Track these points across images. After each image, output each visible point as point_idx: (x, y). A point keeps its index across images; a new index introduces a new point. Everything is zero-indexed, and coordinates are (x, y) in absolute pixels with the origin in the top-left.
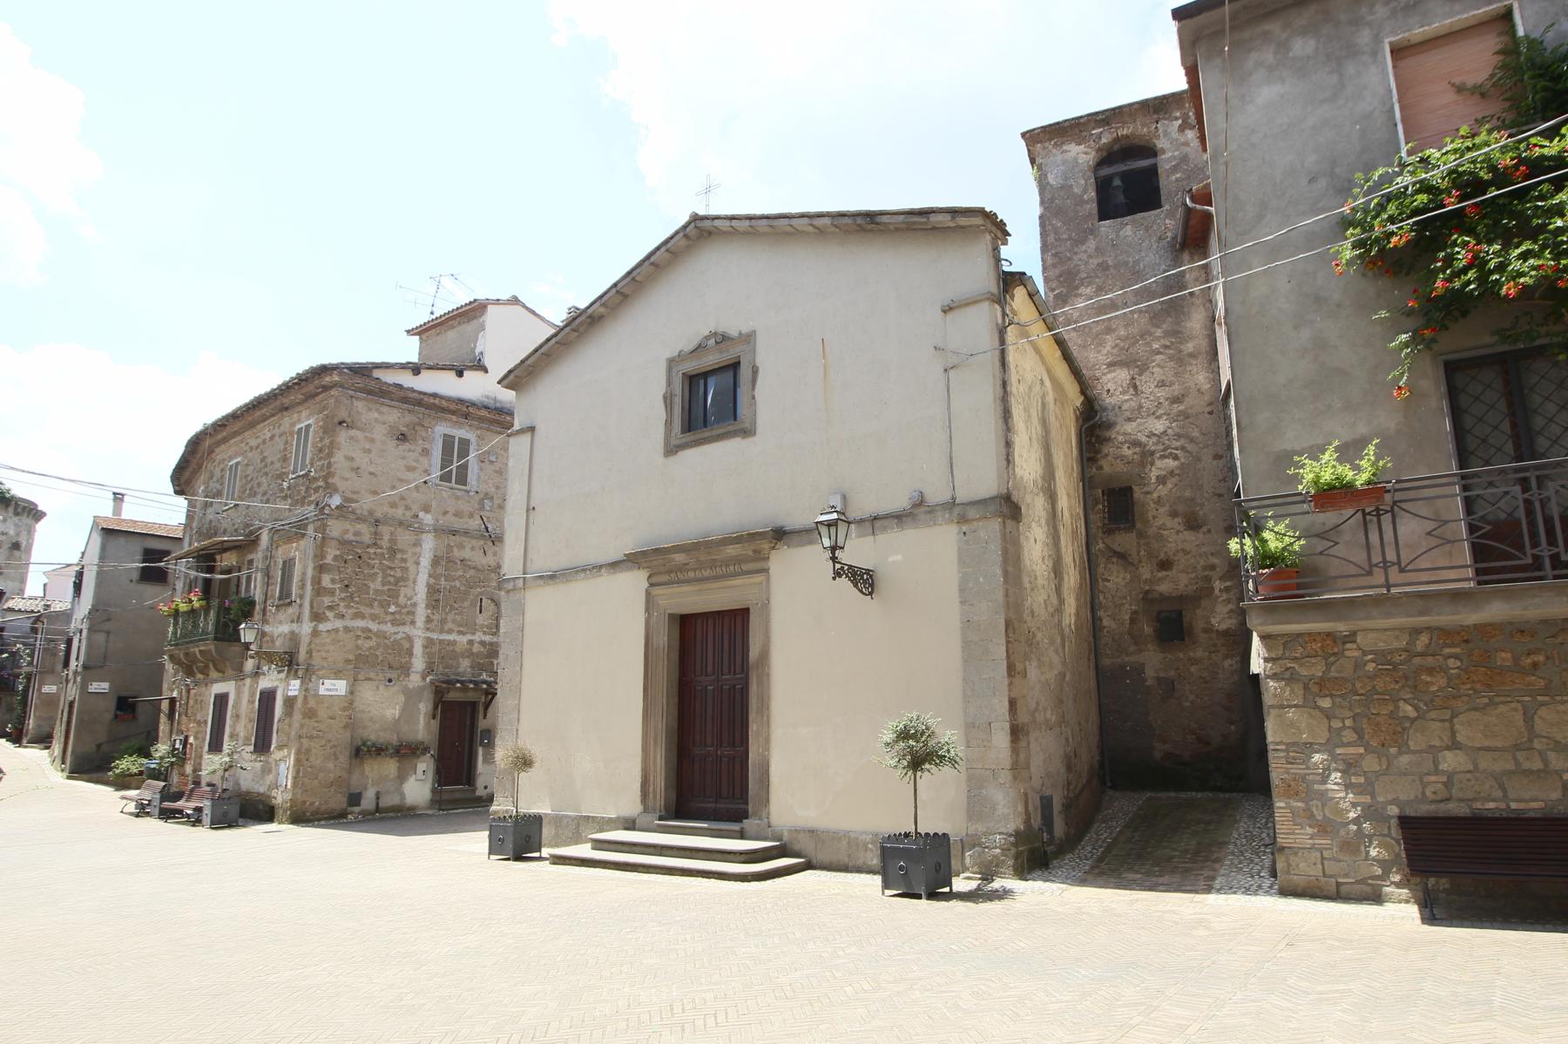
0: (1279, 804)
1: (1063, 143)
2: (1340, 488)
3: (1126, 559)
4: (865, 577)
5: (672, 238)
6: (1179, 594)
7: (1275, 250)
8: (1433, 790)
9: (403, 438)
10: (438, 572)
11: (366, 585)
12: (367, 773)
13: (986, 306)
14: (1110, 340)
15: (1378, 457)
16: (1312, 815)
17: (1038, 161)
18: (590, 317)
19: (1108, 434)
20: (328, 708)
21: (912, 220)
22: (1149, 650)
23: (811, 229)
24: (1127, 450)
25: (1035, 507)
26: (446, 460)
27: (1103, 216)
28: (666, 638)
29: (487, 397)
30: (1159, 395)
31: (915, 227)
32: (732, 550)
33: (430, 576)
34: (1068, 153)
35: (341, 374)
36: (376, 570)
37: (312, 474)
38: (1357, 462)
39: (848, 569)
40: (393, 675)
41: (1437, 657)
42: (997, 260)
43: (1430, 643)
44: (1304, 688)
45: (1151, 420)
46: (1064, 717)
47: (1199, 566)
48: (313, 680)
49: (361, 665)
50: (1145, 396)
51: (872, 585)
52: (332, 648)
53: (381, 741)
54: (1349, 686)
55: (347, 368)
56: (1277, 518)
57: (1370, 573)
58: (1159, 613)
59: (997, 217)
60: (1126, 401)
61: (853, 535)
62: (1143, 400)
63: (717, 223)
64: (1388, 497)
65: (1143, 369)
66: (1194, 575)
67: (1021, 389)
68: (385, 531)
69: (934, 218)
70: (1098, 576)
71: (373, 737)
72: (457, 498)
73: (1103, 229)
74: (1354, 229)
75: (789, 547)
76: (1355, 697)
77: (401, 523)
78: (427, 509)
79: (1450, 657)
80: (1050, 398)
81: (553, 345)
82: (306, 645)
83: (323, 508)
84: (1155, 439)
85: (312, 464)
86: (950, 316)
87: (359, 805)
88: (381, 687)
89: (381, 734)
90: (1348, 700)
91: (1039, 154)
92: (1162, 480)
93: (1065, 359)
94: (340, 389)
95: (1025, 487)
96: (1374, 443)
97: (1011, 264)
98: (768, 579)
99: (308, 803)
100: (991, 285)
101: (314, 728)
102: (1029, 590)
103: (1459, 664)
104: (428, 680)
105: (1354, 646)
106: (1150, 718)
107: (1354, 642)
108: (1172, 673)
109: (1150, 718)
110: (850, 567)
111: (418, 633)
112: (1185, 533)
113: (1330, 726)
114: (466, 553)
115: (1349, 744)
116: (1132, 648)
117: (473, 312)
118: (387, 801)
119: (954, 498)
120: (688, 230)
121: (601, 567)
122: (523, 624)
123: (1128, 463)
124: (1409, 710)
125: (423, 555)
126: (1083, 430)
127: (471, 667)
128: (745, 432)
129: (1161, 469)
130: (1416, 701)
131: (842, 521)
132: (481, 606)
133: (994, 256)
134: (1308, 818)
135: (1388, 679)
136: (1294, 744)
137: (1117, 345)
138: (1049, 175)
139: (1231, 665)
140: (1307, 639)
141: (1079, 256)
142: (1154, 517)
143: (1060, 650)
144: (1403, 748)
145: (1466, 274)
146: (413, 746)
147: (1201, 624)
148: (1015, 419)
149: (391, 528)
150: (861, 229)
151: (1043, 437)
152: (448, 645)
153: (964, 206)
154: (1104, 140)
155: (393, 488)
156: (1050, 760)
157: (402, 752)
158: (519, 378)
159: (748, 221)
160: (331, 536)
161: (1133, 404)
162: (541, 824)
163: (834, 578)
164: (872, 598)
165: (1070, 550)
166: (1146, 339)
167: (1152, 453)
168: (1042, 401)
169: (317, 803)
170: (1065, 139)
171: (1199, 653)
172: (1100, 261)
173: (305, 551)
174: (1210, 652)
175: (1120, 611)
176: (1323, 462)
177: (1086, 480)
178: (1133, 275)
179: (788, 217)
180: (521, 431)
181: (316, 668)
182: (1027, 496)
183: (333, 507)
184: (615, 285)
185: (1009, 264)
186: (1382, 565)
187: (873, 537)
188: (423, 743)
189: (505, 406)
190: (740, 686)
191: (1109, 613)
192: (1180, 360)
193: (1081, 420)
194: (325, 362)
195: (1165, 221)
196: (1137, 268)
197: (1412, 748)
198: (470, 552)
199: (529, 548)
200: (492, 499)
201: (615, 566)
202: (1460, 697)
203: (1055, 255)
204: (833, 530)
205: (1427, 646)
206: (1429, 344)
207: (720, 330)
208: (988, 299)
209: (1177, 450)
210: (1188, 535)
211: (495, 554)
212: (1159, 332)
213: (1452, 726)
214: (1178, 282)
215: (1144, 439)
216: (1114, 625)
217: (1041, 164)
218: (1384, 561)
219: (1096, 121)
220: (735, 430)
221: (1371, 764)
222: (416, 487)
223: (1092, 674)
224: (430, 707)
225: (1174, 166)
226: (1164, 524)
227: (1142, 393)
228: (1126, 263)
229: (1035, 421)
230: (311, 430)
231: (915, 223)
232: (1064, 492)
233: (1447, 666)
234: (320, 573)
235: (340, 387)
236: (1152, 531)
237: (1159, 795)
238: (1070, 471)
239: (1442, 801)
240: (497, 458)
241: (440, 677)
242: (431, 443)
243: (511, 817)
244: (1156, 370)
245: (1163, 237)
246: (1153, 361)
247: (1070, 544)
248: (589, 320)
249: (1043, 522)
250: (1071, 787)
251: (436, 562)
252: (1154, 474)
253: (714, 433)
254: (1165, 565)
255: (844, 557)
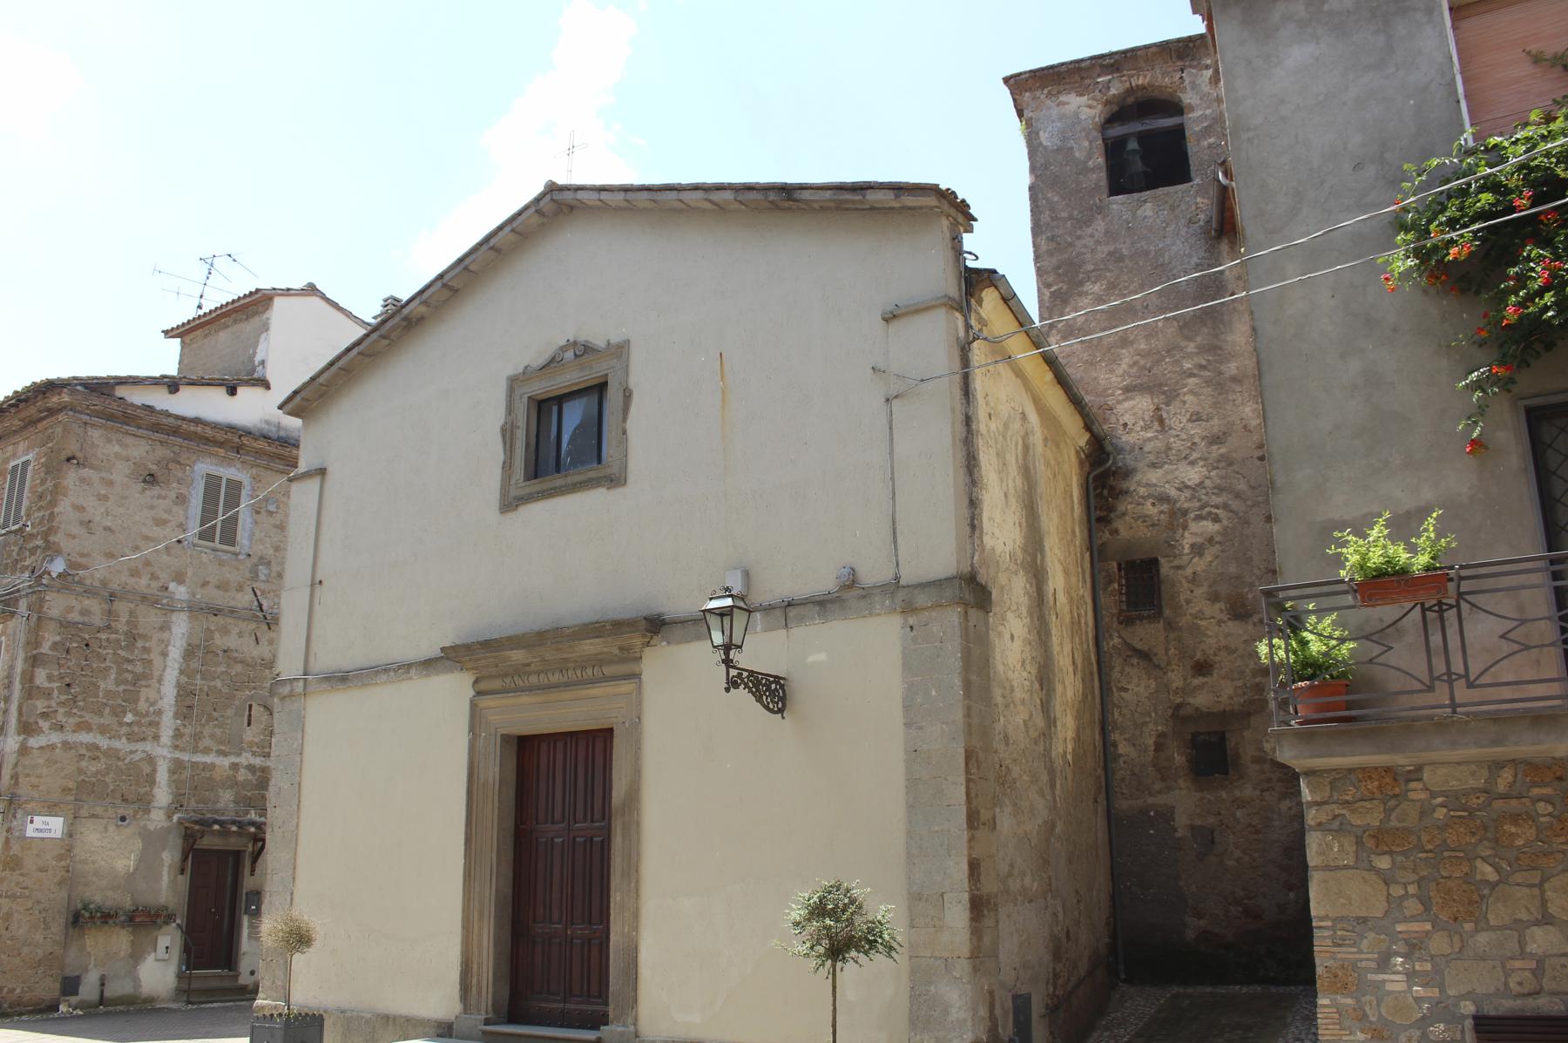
0: (1322, 1001)
1: (1059, 92)
2: (1393, 575)
3: (1151, 660)
4: (773, 686)
5: (520, 213)
6: (1222, 709)
7: (1314, 255)
8: (1519, 980)
9: (151, 479)
10: (192, 667)
11: (94, 684)
12: (89, 949)
13: (941, 315)
14: (1126, 357)
15: (1440, 534)
16: (1365, 1015)
17: (1027, 114)
18: (406, 319)
19: (1125, 485)
20: (37, 855)
21: (842, 197)
22: (1181, 789)
23: (708, 205)
24: (1151, 507)
25: (1013, 590)
26: (208, 512)
27: (1116, 188)
28: (497, 769)
29: (267, 422)
30: (1192, 432)
31: (847, 206)
32: (589, 647)
33: (182, 672)
34: (1066, 106)
35: (73, 392)
36: (108, 663)
37: (28, 529)
38: (1413, 540)
39: (748, 677)
40: (128, 811)
41: (1523, 800)
42: (958, 251)
43: (1515, 782)
44: (1357, 843)
45: (1183, 466)
46: (1050, 885)
47: (1247, 671)
48: (19, 816)
49: (84, 797)
50: (1172, 432)
51: (783, 699)
52: (45, 771)
53: (109, 903)
54: (1413, 839)
55: (80, 384)
56: (1321, 612)
57: (1430, 688)
58: (1195, 735)
59: (956, 197)
60: (1150, 439)
61: (759, 628)
62: (1172, 440)
63: (580, 195)
64: (1451, 586)
65: (1171, 396)
66: (1239, 683)
67: (993, 427)
68: (122, 608)
69: (871, 196)
70: (1112, 685)
71: (98, 898)
72: (221, 563)
73: (1115, 206)
74: (1406, 234)
75: (669, 643)
76: (1421, 855)
77: (144, 598)
78: (180, 578)
79: (1539, 800)
80: (1037, 438)
81: (355, 356)
82: (10, 767)
83: (40, 576)
84: (1188, 493)
85: (28, 516)
86: (895, 326)
87: (76, 993)
88: (111, 828)
89: (110, 893)
90: (1412, 858)
91: (1028, 105)
92: (1198, 550)
93: (1059, 383)
94: (71, 413)
95: (998, 561)
96: (1434, 515)
97: (977, 258)
98: (640, 688)
99: (6, 989)
100: (951, 286)
101: (17, 884)
102: (1001, 708)
103: (1550, 809)
104: (175, 818)
105: (1419, 785)
106: (1182, 883)
107: (1419, 780)
108: (1212, 820)
109: (1182, 883)
110: (751, 673)
111: (163, 752)
112: (1230, 624)
113: (1389, 894)
114: (232, 641)
115: (1413, 918)
116: (1158, 786)
117: (255, 305)
118: (115, 989)
119: (897, 578)
120: (542, 203)
121: (410, 666)
122: (302, 744)
123: (1153, 525)
124: (1488, 872)
125: (172, 643)
126: (1091, 480)
127: (234, 801)
128: (612, 481)
129: (1196, 534)
130: (1497, 860)
131: (743, 607)
132: (250, 715)
133: (953, 248)
134: (1360, 1020)
135: (1462, 829)
136: (1342, 919)
137: (1135, 363)
138: (1041, 133)
139: (1290, 808)
140: (1360, 776)
141: (1083, 242)
142: (1188, 602)
143: (1047, 791)
144: (1481, 924)
145: (1542, 298)
146: (153, 912)
147: (1248, 752)
148: (983, 468)
149: (130, 605)
150: (775, 206)
151: (1024, 492)
152: (203, 770)
153: (912, 181)
154: (1113, 91)
155: (136, 548)
156: (1029, 944)
157: (138, 920)
158: (307, 401)
159: (622, 194)
160: (50, 616)
161: (1158, 444)
162: (322, 1026)
163: (727, 690)
164: (783, 718)
165: (1067, 649)
166: (1174, 356)
167: (1185, 513)
168: (1024, 442)
169: (18, 990)
170: (1062, 88)
171: (1248, 791)
172: (1112, 248)
173: (14, 635)
174: (1262, 791)
175: (1142, 732)
176: (1371, 539)
177: (1095, 549)
178: (1156, 268)
179: (676, 189)
180: (308, 475)
181: (23, 799)
182: (1000, 575)
183: (54, 575)
184: (441, 276)
185: (974, 258)
186: (1445, 678)
187: (785, 631)
188: (167, 908)
189: (293, 434)
190: (600, 839)
191: (1126, 736)
192: (1220, 385)
193: (1087, 465)
194: (53, 376)
195: (1193, 200)
196: (1161, 259)
197: (1492, 923)
198: (237, 639)
199: (314, 637)
200: (269, 564)
201: (428, 665)
202: (1552, 853)
203: (1052, 239)
204: (727, 620)
205: (1511, 785)
206: (1507, 384)
207: (582, 338)
208: (945, 305)
209: (1218, 508)
210: (1233, 627)
211: (271, 642)
212: (1191, 347)
213: (1543, 893)
214: (1214, 282)
215: (1173, 493)
216: (1133, 754)
217: (1031, 118)
218: (1449, 672)
219: (1102, 66)
220: (598, 478)
221: (1439, 943)
222: (167, 548)
223: (1101, 822)
224: (178, 856)
225: (1206, 127)
226: (1201, 611)
227: (1170, 429)
228: (1147, 253)
229: (1013, 470)
230: (30, 468)
231: (847, 201)
232: (1059, 568)
233: (1536, 811)
234: (33, 667)
235: (71, 410)
236: (1184, 621)
237: (1190, 990)
238: (1069, 537)
239: (1529, 994)
240: (278, 507)
241: (192, 814)
242: (188, 487)
243: (280, 1015)
244: (1189, 398)
245: (1194, 219)
246: (1185, 386)
247: (1067, 641)
248: (404, 323)
249: (1024, 611)
250: (1060, 982)
251: (189, 653)
252: (1187, 541)
253: (570, 480)
254: (1202, 668)
255: (742, 659)
